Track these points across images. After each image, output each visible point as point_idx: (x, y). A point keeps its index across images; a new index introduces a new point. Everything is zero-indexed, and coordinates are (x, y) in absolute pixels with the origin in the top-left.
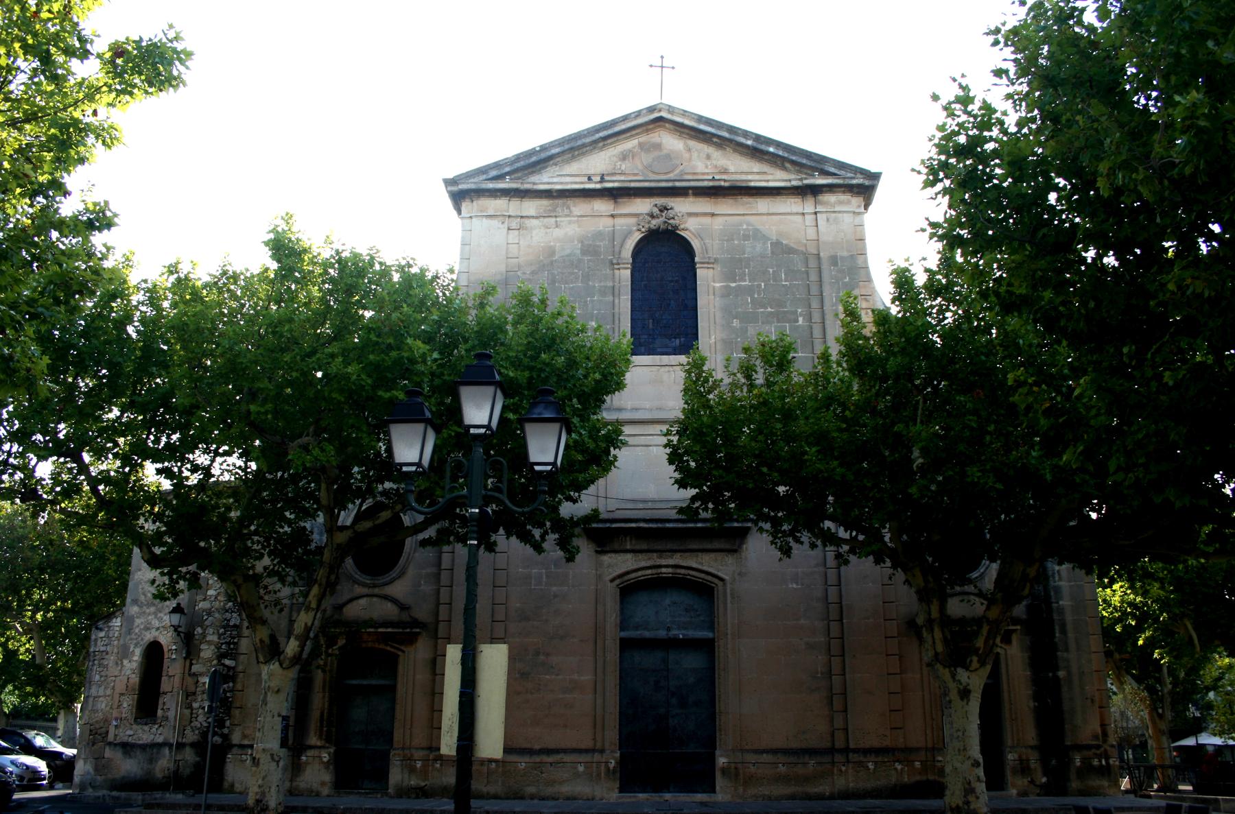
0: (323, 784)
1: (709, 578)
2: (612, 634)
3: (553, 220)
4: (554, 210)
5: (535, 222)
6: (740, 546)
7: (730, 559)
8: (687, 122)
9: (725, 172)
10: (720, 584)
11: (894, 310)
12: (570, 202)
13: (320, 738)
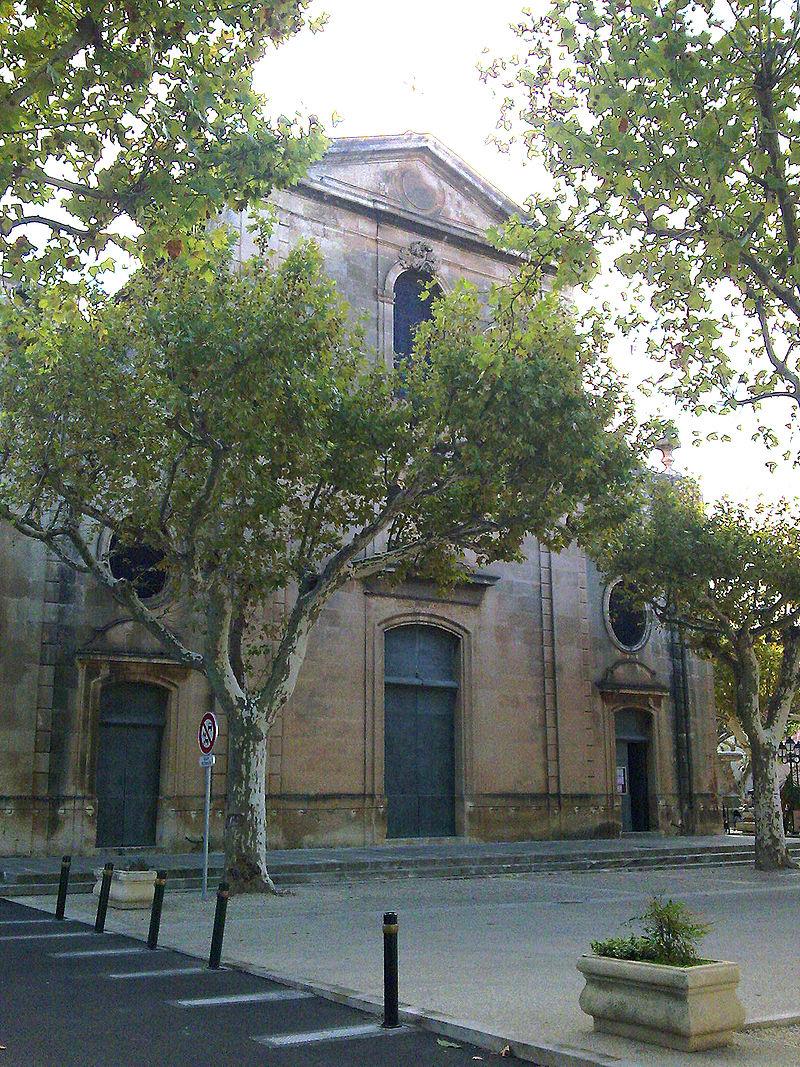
1: (457, 629)
2: (380, 678)
6: (480, 600)
8: (449, 162)
9: (472, 226)
11: (267, 40)
12: (338, 211)
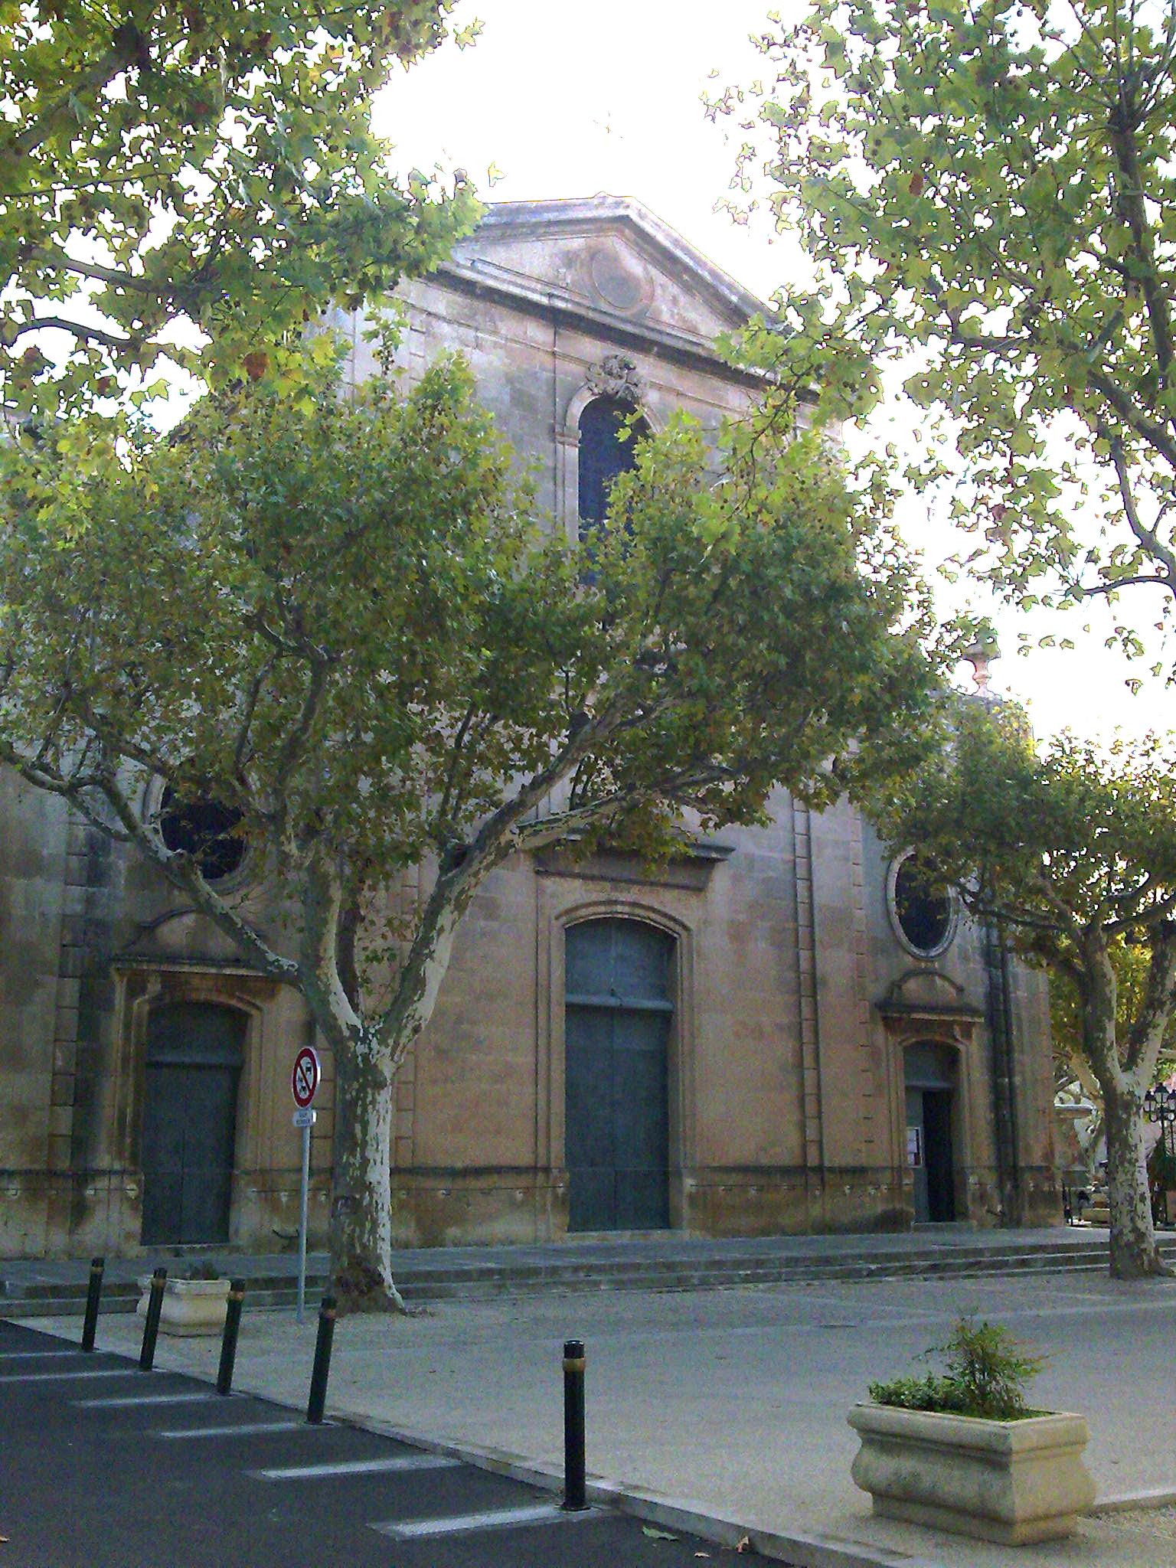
0: (129, 1236)
2: (558, 995)
3: (472, 333)
4: (472, 317)
5: (446, 328)
7: (694, 901)
9: (694, 331)
10: (684, 934)
12: (497, 311)
13: (120, 1155)
